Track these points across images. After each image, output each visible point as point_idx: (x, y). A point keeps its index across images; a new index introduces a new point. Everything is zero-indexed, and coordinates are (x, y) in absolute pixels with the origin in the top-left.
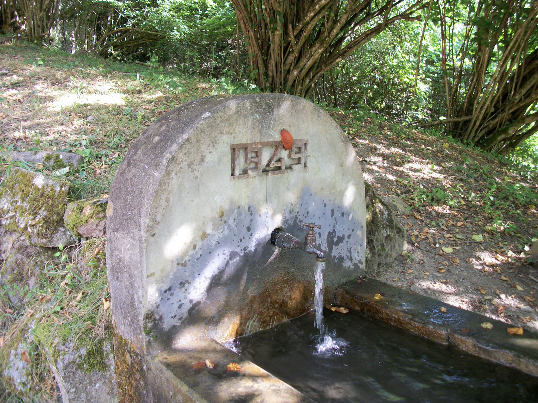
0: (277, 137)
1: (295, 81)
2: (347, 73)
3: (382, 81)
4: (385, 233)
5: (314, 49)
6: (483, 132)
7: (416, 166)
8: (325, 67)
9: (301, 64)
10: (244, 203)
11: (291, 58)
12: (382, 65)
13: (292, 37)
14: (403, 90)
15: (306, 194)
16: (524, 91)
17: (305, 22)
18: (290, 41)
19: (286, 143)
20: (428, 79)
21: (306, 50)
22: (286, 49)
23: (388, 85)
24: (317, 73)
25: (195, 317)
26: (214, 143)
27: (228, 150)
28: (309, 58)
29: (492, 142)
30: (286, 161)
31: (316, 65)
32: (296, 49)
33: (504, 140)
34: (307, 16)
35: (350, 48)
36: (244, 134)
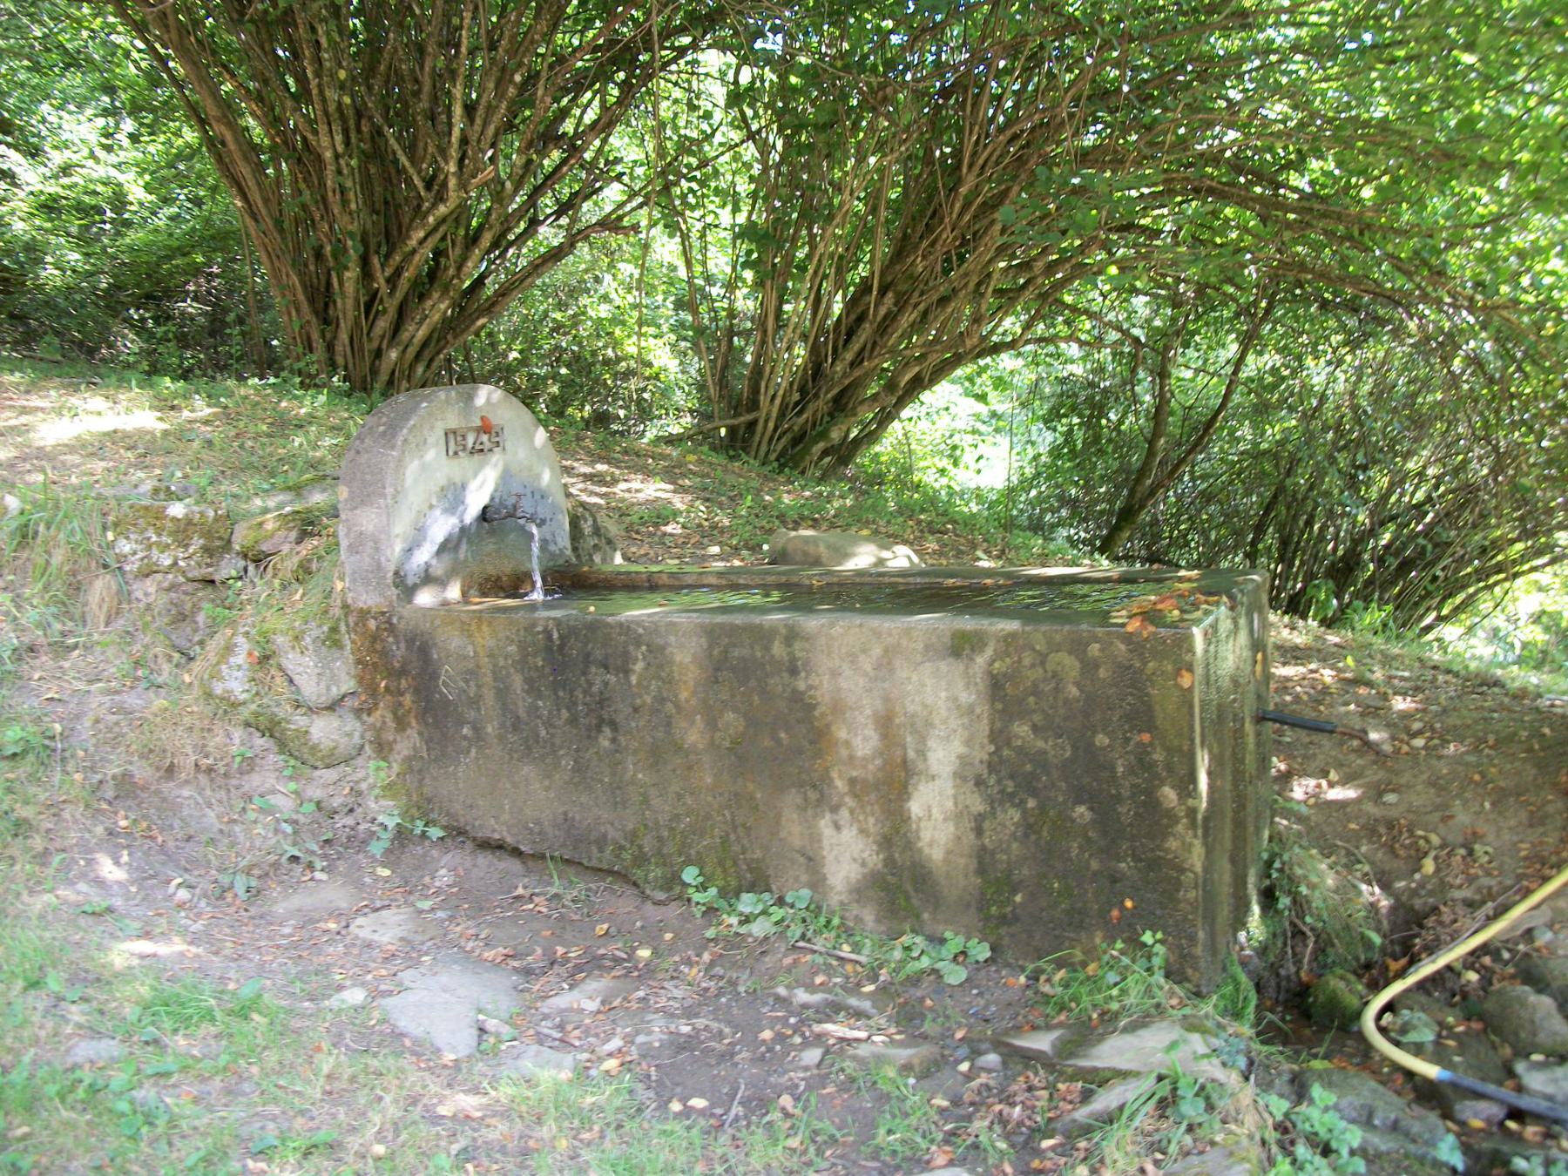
0: (478, 423)
1: (393, 372)
2: (492, 345)
3: (577, 358)
4: (592, 541)
5: (430, 303)
6: (784, 440)
7: (635, 485)
8: (455, 338)
9: (405, 336)
10: (458, 480)
11: (383, 324)
12: (576, 320)
13: (382, 281)
14: (628, 374)
15: (506, 476)
16: (849, 356)
17: (407, 249)
18: (378, 290)
19: (486, 428)
20: (683, 344)
21: (411, 304)
22: (370, 304)
23: (593, 364)
24: (438, 353)
25: (428, 579)
26: (432, 428)
27: (442, 434)
28: (420, 323)
29: (803, 458)
30: (487, 445)
31: (436, 335)
32: (392, 305)
33: (825, 453)
34: (409, 237)
35: (503, 295)
36: (453, 421)
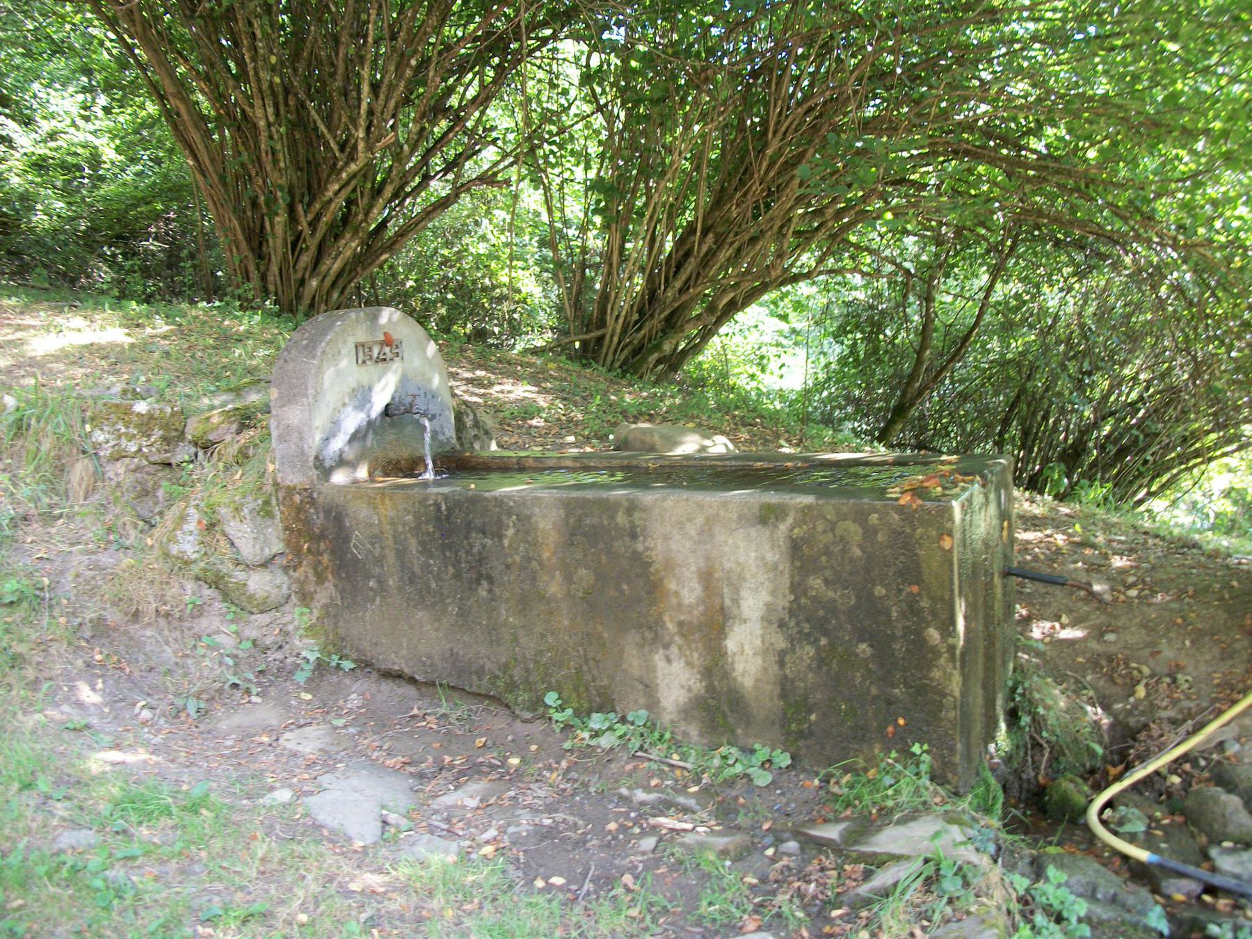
0: (382, 338)
1: (314, 297)
2: (393, 275)
3: (461, 286)
4: (473, 432)
5: (343, 242)
6: (626, 352)
7: (507, 387)
8: (363, 270)
9: (323, 268)
10: (365, 383)
11: (305, 259)
12: (460, 256)
13: (305, 224)
14: (501, 299)
15: (404, 380)
16: (678, 284)
17: (325, 199)
18: (302, 231)
19: (388, 342)
20: (545, 274)
21: (328, 243)
22: (296, 243)
23: (474, 291)
24: (350, 282)
25: (341, 462)
26: (345, 342)
27: (353, 346)
28: (336, 258)
29: (641, 366)
30: (389, 355)
31: (348, 268)
32: (313, 244)
33: (659, 362)
34: (327, 190)
35: (402, 235)
36: (362, 336)
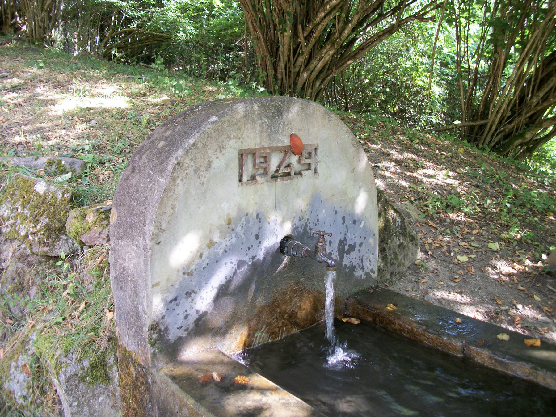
0: (287, 142)
1: (305, 84)
2: (358, 76)
3: (394, 84)
4: (397, 241)
5: (325, 50)
6: (500, 136)
7: (430, 172)
8: (336, 69)
9: (312, 66)
10: (252, 210)
11: (301, 60)
12: (395, 67)
13: (302, 38)
14: (416, 93)
15: (316, 201)
16: (541, 94)
17: (315, 22)
18: (300, 42)
19: (295, 148)
20: (442, 82)
21: (316, 51)
22: (296, 51)
23: (401, 88)
24: (328, 76)
25: (201, 328)
26: (221, 148)
27: (236, 155)
28: (320, 60)
29: (509, 147)
30: (296, 166)
31: (327, 67)
32: (306, 51)
33: (521, 145)
34: (317, 16)
35: (362, 49)
36: (252, 138)
